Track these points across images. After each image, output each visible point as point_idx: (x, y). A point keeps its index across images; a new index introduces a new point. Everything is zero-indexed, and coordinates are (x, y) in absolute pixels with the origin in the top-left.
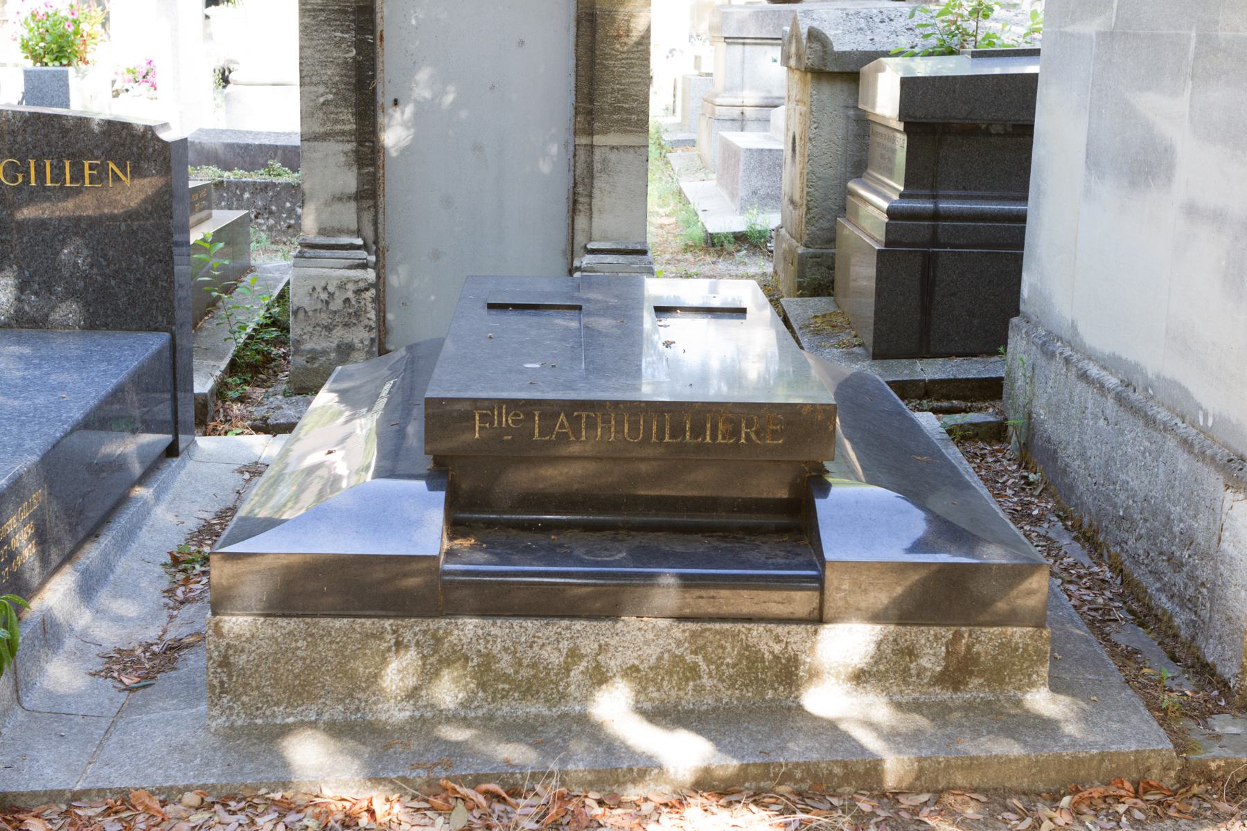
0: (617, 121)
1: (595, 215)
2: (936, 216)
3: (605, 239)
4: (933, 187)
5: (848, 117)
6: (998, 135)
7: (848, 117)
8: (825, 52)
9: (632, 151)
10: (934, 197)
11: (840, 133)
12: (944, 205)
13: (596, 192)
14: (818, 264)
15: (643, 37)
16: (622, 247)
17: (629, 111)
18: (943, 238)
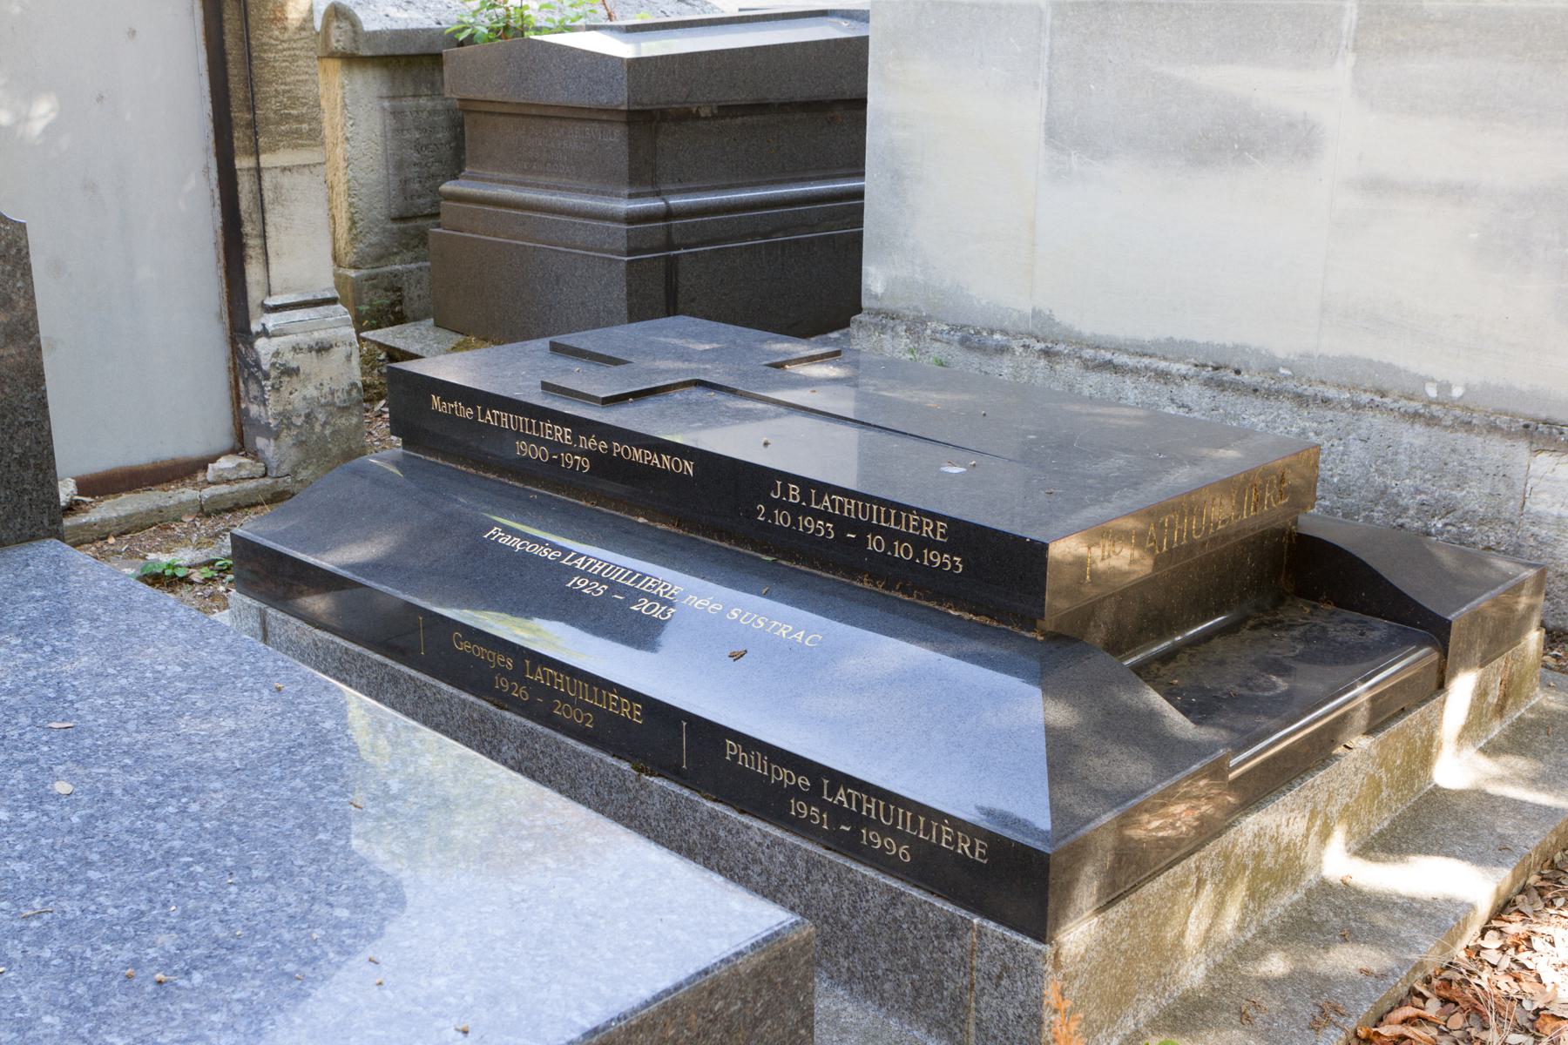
0: (287, 133)
1: (272, 260)
2: (669, 214)
3: (287, 290)
4: (653, 184)
5: (383, 109)
6: (706, 118)
7: (383, 109)
8: (355, 32)
9: (306, 171)
10: (658, 194)
11: (378, 129)
12: (677, 201)
13: (270, 230)
14: (375, 287)
15: (305, 20)
16: (309, 297)
17: (299, 119)
18: (676, 239)
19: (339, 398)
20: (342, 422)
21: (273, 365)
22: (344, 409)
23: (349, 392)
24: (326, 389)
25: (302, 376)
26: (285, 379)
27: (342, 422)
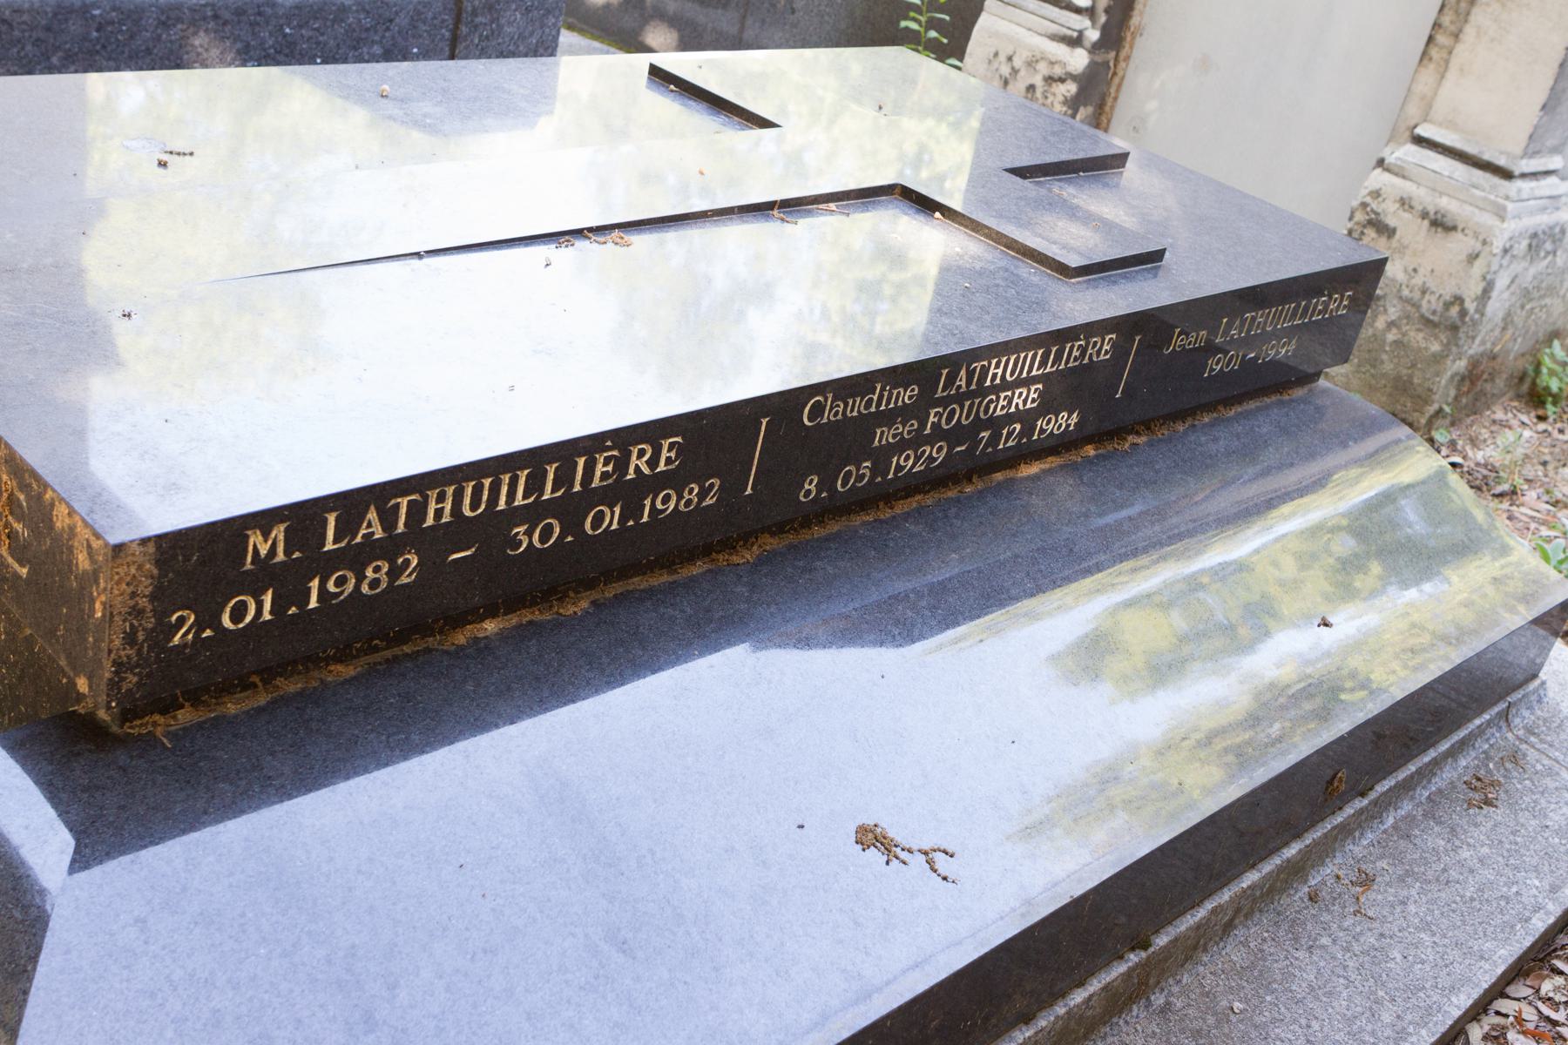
3: (1450, 124)
19: (1430, 304)
20: (1417, 338)
21: (1364, 205)
22: (1428, 322)
23: (1448, 305)
24: (1418, 281)
25: (1394, 242)
26: (1371, 233)
27: (1417, 338)
